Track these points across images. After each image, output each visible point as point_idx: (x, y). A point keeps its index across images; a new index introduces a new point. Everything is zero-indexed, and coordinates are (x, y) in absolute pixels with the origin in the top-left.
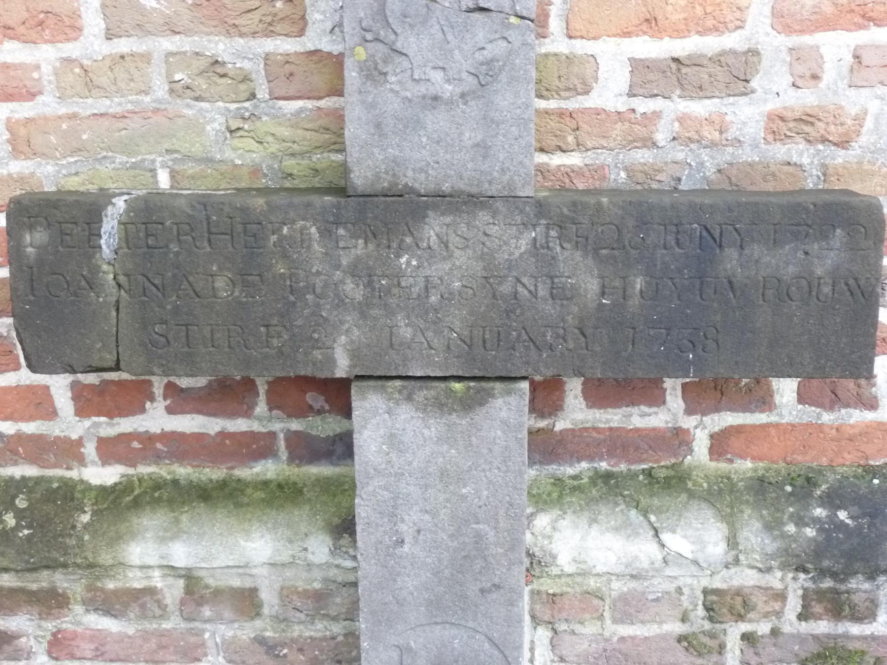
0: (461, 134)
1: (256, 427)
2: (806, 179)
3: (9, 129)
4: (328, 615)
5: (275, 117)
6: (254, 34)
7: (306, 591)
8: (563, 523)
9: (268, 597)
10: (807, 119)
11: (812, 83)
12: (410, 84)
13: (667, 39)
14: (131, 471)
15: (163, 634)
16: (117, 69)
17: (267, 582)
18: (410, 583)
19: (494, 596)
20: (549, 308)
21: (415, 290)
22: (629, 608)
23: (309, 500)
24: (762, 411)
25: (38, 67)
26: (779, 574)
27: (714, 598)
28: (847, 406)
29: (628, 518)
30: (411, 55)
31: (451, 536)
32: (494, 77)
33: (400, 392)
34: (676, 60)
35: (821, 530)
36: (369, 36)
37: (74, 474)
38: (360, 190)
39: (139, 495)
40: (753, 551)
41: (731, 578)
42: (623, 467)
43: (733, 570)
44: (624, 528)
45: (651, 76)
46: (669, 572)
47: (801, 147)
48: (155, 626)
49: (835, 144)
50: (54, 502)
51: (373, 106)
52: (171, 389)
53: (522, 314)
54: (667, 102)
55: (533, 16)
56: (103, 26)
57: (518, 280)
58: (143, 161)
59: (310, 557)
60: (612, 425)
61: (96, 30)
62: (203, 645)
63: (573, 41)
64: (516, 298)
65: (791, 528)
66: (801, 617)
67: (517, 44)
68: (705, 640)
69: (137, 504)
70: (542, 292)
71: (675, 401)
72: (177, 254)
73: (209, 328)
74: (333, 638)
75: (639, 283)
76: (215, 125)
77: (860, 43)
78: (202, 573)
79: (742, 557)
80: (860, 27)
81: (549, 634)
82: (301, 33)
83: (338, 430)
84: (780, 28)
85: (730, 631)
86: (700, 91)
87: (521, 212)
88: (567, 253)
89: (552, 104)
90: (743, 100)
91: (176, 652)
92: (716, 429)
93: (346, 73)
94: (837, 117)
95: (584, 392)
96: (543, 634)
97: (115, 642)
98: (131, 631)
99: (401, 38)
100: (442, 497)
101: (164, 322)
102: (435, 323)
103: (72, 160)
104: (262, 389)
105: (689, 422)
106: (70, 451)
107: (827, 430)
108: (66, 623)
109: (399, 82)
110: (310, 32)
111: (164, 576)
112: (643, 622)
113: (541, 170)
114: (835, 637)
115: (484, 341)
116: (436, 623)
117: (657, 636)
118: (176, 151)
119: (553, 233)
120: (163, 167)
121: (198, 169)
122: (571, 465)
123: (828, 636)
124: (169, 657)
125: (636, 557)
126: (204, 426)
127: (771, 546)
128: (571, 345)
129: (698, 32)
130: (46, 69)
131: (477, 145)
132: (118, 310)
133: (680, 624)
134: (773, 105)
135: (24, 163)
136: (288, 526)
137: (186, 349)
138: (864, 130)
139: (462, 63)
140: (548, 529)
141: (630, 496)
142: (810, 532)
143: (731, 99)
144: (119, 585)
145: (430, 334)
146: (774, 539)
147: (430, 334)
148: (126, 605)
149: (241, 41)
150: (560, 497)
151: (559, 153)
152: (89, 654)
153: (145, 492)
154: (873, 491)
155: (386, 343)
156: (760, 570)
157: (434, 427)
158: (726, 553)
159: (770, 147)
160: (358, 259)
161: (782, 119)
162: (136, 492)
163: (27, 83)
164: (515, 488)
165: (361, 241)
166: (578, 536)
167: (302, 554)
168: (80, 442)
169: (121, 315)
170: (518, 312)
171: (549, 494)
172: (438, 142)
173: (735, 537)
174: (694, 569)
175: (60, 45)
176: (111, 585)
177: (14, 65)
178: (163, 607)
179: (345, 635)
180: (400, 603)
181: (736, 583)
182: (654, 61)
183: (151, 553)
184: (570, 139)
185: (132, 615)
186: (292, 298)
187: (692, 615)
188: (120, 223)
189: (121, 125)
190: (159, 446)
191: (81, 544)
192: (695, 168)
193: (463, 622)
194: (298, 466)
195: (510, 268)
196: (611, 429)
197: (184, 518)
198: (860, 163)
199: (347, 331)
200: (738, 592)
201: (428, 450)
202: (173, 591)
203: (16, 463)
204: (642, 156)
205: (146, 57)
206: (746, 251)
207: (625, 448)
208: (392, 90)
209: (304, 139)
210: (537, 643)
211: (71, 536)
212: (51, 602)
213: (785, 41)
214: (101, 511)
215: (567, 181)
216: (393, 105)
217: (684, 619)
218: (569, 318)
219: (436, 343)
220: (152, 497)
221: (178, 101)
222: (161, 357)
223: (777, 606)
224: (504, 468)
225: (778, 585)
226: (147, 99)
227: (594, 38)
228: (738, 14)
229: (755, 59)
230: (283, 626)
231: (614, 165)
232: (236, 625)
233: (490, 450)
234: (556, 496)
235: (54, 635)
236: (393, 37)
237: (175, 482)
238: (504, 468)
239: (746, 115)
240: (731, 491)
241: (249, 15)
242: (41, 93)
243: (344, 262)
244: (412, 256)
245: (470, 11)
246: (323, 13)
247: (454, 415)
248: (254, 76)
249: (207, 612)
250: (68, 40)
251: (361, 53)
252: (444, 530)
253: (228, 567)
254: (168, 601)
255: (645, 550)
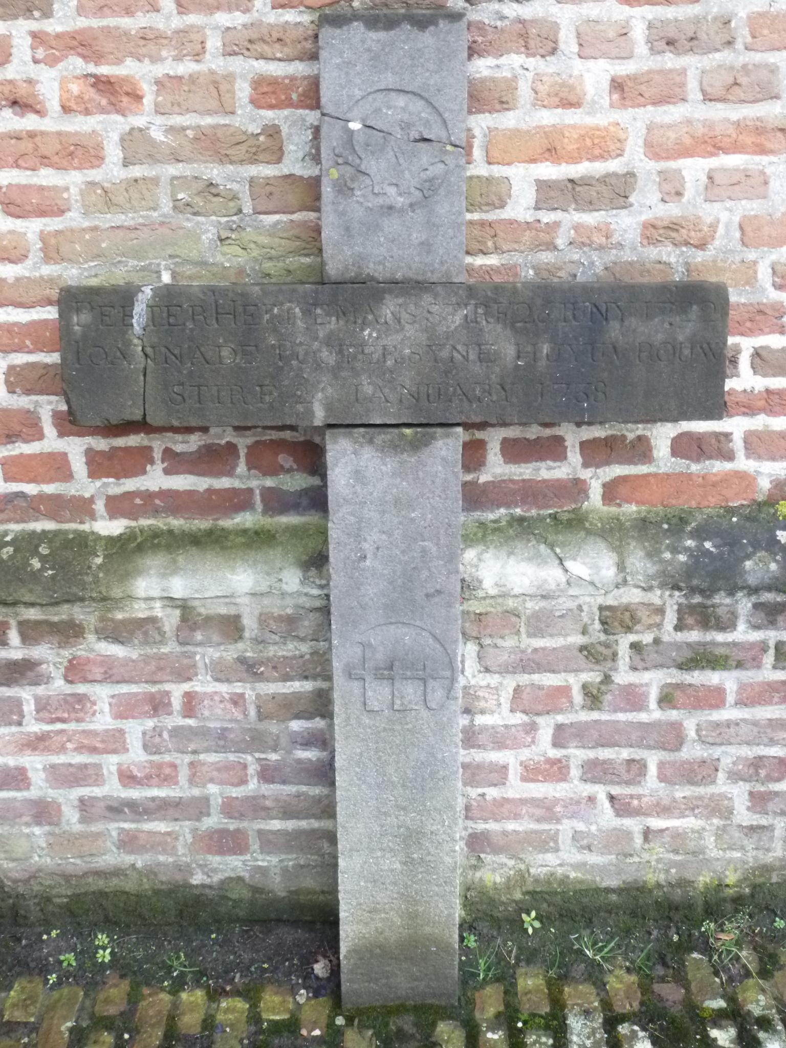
0: (410, 235)
1: (237, 484)
2: (673, 274)
3: (42, 239)
4: (297, 637)
5: (256, 228)
6: (242, 162)
7: (280, 616)
8: (487, 556)
9: (249, 623)
10: (673, 227)
11: (676, 198)
12: (371, 197)
13: (564, 164)
14: (133, 524)
15: (160, 657)
16: (131, 190)
17: (248, 609)
18: (371, 590)
19: (436, 599)
20: (477, 369)
21: (375, 356)
22: (540, 624)
23: (281, 543)
24: (644, 464)
25: (67, 189)
26: (658, 592)
27: (608, 613)
28: (710, 458)
29: (539, 551)
30: (372, 175)
31: (403, 552)
32: (435, 191)
33: (363, 437)
34: (571, 181)
35: (691, 556)
36: (340, 161)
37: (86, 527)
38: (333, 279)
39: (142, 542)
40: (638, 573)
41: (621, 596)
42: (534, 512)
43: (622, 590)
44: (536, 558)
45: (552, 194)
46: (572, 592)
47: (669, 249)
48: (155, 650)
49: (695, 247)
50: (72, 549)
51: (343, 214)
52: (168, 453)
53: (457, 374)
54: (566, 215)
55: (464, 145)
56: (121, 156)
57: (454, 348)
58: (150, 264)
59: (284, 586)
60: (525, 477)
61: (115, 160)
62: (194, 666)
63: (492, 167)
64: (452, 361)
65: (667, 555)
66: (678, 628)
67: (452, 166)
68: (601, 649)
69: (140, 549)
70: (472, 356)
71: (574, 457)
72: (192, 330)
73: (215, 388)
74: (302, 657)
75: (545, 349)
76: (209, 235)
77: (712, 166)
78: (196, 603)
79: (629, 578)
80: (712, 155)
81: (476, 648)
82: (279, 161)
83: (304, 486)
84: (651, 156)
85: (621, 641)
86: (590, 205)
87: (456, 294)
88: (490, 326)
89: (476, 216)
90: (623, 212)
91: (172, 673)
92: (608, 479)
93: (323, 188)
94: (696, 224)
95: (501, 449)
96: (471, 649)
97: (122, 665)
98: (135, 656)
99: (365, 162)
100: (396, 520)
101: (182, 384)
102: (390, 382)
103: (92, 264)
104: (242, 452)
105: (586, 474)
106: (82, 507)
107: (695, 478)
108: (80, 651)
109: (363, 196)
110: (286, 160)
111: (164, 607)
112: (551, 636)
113: (470, 270)
114: (704, 644)
115: (428, 396)
116: (391, 623)
117: (563, 647)
118: (177, 256)
119: (480, 311)
120: (166, 269)
121: (194, 271)
122: (492, 512)
123: (699, 643)
124: (166, 678)
125: (545, 581)
126: (195, 484)
127: (652, 569)
128: (495, 398)
129: (588, 159)
130: (74, 190)
131: (422, 243)
132: (145, 375)
133: (580, 636)
134: (646, 216)
135: (53, 267)
136: (266, 562)
137: (198, 405)
138: (717, 235)
139: (410, 180)
140: (475, 560)
141: (539, 534)
142: (682, 558)
143: (614, 212)
144: (127, 615)
145: (387, 391)
146: (654, 564)
147: (387, 391)
148: (132, 633)
149: (231, 167)
150: (484, 536)
151: (481, 255)
152: (99, 677)
153: (146, 540)
154: (732, 526)
155: (353, 398)
156: (644, 589)
157: (390, 464)
158: (617, 575)
159: (645, 250)
160: (331, 332)
161: (654, 227)
162: (139, 540)
163: (59, 202)
164: (452, 512)
165: (334, 319)
166: (499, 565)
167: (277, 585)
168: (92, 500)
169: (148, 378)
170: (454, 372)
171: (475, 534)
172: (392, 241)
173: (623, 562)
174: (591, 589)
175: (85, 171)
176: (119, 616)
177: (48, 187)
178: (162, 633)
179: (312, 654)
180: (363, 607)
181: (625, 600)
182: (555, 181)
183: (154, 588)
184: (490, 244)
185: (136, 641)
186: (280, 364)
187: (590, 629)
188: (148, 306)
189: (133, 236)
190: (157, 502)
191: (97, 581)
192: (589, 266)
193: (412, 622)
194: (271, 516)
195: (447, 338)
196: (524, 480)
197: (180, 559)
198: (714, 261)
199: (323, 389)
200: (627, 608)
201: (385, 483)
202: (170, 619)
203: (37, 520)
204: (546, 257)
205: (155, 181)
206: (626, 323)
207: (535, 496)
208: (358, 202)
209: (280, 246)
210: (467, 656)
211: (87, 574)
212: (69, 632)
213: (654, 166)
214: (111, 555)
215: (487, 277)
216: (358, 213)
217: (584, 632)
218: (493, 377)
219: (391, 397)
220: (152, 543)
221: (180, 216)
222: (178, 411)
223: (657, 619)
224: (443, 496)
225: (658, 601)
226: (155, 214)
227: (508, 164)
228: (618, 145)
229: (632, 180)
230: (261, 647)
231: (525, 265)
232: (222, 648)
233: (433, 482)
234: (483, 535)
235: (70, 661)
236: (358, 161)
237: (171, 532)
238: (443, 496)
239: (626, 224)
240: (620, 530)
241: (238, 147)
242: (69, 210)
243: (321, 334)
244: (373, 330)
245: (416, 141)
246: (297, 145)
247: (405, 455)
248: (240, 195)
249: (199, 636)
250: (92, 167)
251: (334, 173)
252: (397, 547)
253: (217, 597)
254: (167, 628)
255: (552, 575)
